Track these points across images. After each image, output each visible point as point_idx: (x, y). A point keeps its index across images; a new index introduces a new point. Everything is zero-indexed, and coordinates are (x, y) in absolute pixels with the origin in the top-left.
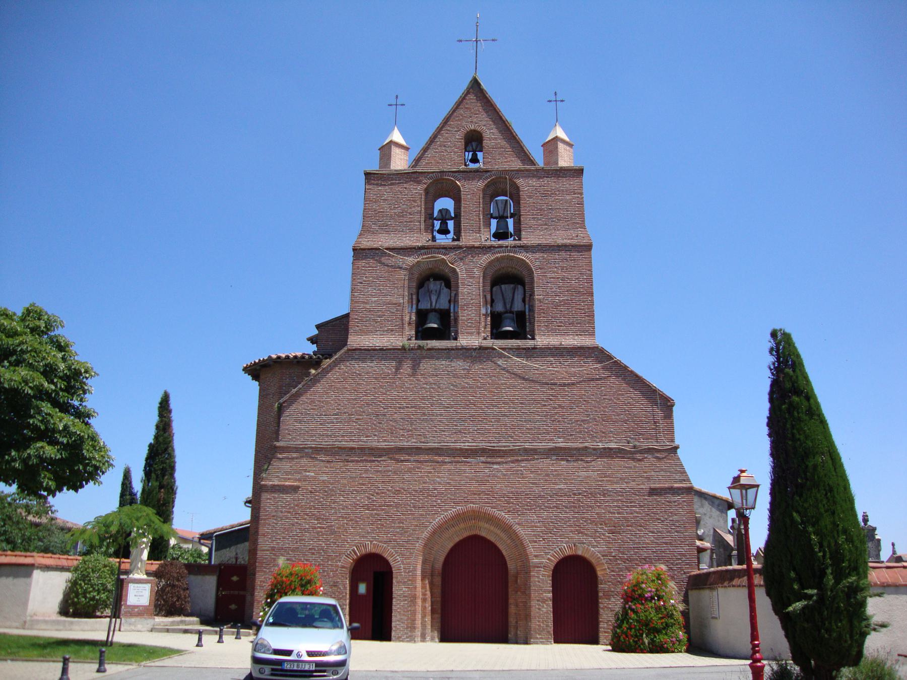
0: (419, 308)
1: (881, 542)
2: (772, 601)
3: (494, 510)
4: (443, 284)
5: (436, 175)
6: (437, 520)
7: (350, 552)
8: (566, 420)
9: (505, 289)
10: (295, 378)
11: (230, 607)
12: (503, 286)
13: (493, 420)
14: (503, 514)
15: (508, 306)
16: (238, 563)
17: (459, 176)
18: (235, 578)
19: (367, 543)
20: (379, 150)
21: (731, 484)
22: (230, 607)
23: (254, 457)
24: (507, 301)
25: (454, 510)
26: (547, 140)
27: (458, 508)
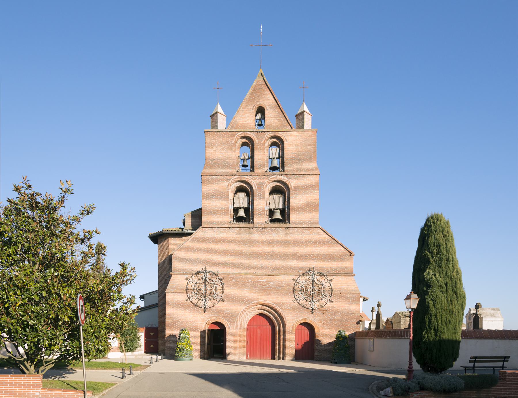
0: (234, 206)
1: (461, 344)
2: (416, 255)
3: (270, 303)
4: (245, 195)
5: (241, 133)
6: (245, 307)
7: (207, 321)
8: (303, 262)
9: (275, 197)
10: (176, 241)
11: (150, 346)
12: (274, 196)
13: (270, 262)
14: (274, 304)
15: (277, 207)
16: (153, 327)
17: (253, 134)
18: (152, 334)
19: (215, 317)
20: (210, 117)
21: (69, 366)
22: (150, 346)
23: (158, 279)
24: (276, 202)
25: (253, 302)
26: (298, 113)
27: (255, 302)
